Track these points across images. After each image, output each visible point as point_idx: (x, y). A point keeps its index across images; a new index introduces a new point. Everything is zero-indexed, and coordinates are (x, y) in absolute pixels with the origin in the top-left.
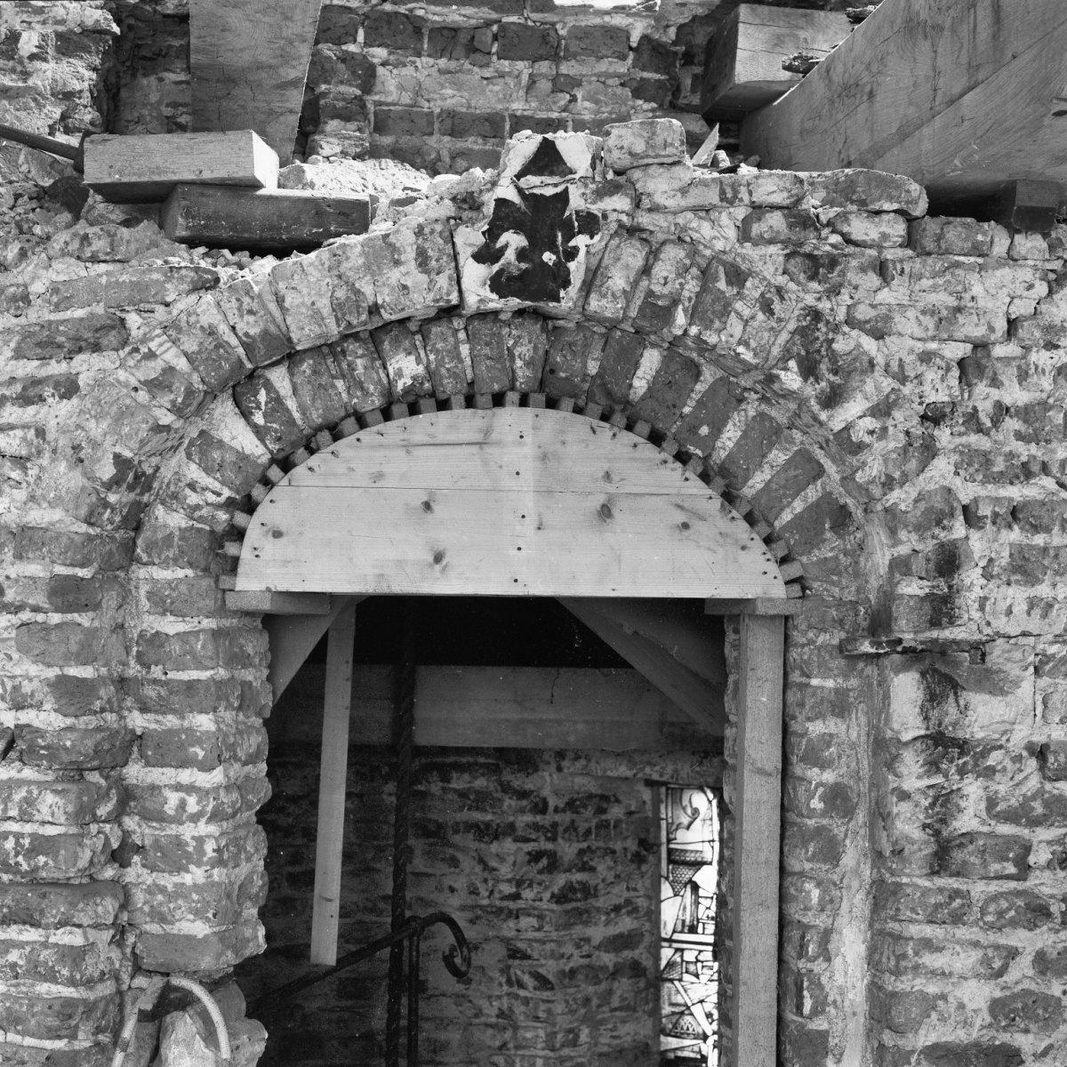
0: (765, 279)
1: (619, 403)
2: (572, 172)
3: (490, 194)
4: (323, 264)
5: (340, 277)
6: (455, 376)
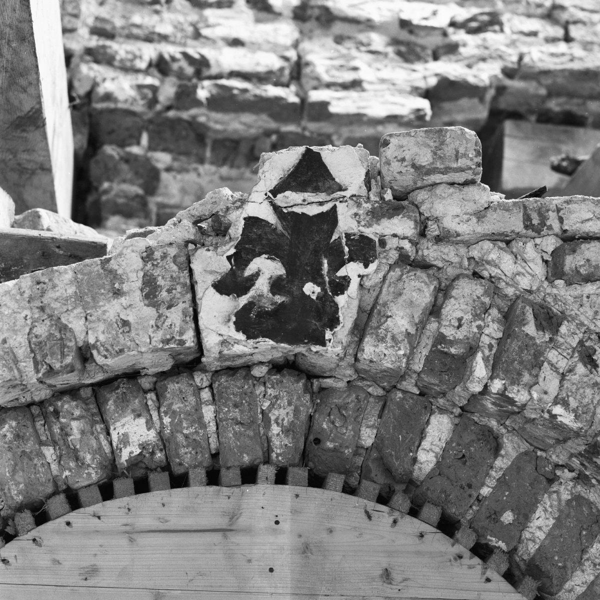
0: (582, 324)
1: (400, 482)
2: (341, 188)
3: (238, 212)
4: (22, 294)
5: (42, 309)
6: (195, 444)
